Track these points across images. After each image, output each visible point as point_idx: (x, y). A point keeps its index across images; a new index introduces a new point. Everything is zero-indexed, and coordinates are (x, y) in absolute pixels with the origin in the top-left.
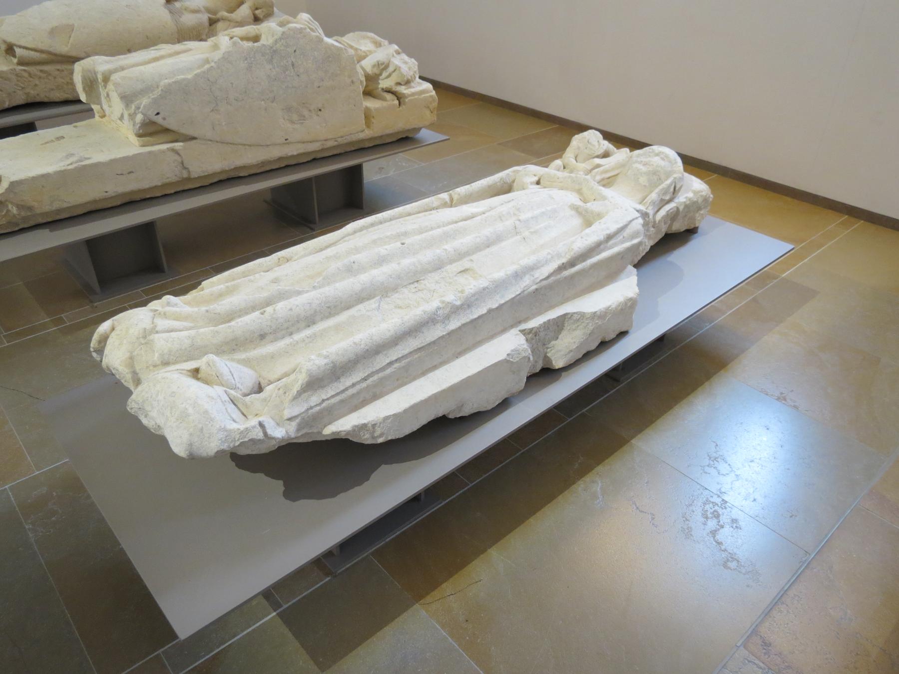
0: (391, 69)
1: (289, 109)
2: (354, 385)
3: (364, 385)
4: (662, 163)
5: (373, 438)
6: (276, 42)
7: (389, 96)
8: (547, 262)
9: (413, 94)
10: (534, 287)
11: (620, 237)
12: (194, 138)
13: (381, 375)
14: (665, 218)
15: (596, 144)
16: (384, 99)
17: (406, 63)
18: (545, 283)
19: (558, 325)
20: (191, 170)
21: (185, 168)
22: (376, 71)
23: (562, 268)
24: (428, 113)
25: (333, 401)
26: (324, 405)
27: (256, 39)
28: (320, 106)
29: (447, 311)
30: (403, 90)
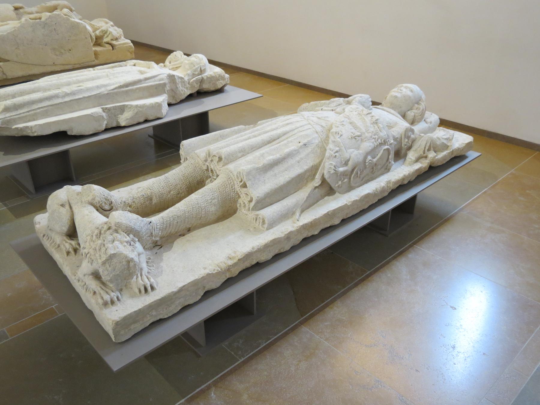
0: (108, 33)
1: (54, 49)
2: (23, 113)
3: (28, 114)
4: (196, 60)
5: (32, 133)
6: (46, 19)
7: (107, 45)
8: (113, 84)
9: (120, 44)
10: (106, 92)
11: (153, 80)
12: (9, 61)
13: (35, 112)
14: (196, 81)
15: (180, 57)
16: (105, 47)
17: (116, 30)
18: (112, 91)
19: (122, 109)
20: (7, 74)
21: (4, 74)
22: (101, 34)
23: (121, 87)
24: (129, 54)
25: (15, 117)
26: (12, 117)
27: (40, 18)
28: (70, 48)
29: (63, 94)
30: (114, 42)
